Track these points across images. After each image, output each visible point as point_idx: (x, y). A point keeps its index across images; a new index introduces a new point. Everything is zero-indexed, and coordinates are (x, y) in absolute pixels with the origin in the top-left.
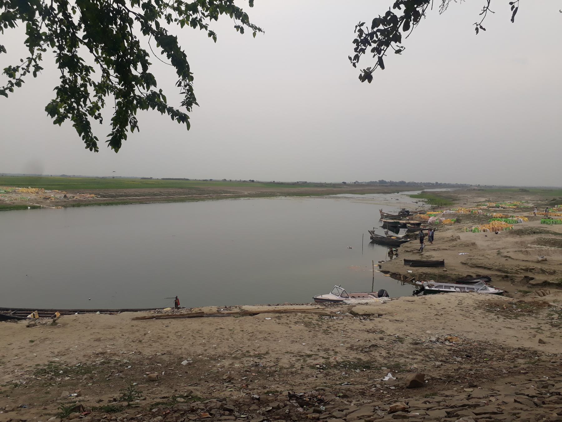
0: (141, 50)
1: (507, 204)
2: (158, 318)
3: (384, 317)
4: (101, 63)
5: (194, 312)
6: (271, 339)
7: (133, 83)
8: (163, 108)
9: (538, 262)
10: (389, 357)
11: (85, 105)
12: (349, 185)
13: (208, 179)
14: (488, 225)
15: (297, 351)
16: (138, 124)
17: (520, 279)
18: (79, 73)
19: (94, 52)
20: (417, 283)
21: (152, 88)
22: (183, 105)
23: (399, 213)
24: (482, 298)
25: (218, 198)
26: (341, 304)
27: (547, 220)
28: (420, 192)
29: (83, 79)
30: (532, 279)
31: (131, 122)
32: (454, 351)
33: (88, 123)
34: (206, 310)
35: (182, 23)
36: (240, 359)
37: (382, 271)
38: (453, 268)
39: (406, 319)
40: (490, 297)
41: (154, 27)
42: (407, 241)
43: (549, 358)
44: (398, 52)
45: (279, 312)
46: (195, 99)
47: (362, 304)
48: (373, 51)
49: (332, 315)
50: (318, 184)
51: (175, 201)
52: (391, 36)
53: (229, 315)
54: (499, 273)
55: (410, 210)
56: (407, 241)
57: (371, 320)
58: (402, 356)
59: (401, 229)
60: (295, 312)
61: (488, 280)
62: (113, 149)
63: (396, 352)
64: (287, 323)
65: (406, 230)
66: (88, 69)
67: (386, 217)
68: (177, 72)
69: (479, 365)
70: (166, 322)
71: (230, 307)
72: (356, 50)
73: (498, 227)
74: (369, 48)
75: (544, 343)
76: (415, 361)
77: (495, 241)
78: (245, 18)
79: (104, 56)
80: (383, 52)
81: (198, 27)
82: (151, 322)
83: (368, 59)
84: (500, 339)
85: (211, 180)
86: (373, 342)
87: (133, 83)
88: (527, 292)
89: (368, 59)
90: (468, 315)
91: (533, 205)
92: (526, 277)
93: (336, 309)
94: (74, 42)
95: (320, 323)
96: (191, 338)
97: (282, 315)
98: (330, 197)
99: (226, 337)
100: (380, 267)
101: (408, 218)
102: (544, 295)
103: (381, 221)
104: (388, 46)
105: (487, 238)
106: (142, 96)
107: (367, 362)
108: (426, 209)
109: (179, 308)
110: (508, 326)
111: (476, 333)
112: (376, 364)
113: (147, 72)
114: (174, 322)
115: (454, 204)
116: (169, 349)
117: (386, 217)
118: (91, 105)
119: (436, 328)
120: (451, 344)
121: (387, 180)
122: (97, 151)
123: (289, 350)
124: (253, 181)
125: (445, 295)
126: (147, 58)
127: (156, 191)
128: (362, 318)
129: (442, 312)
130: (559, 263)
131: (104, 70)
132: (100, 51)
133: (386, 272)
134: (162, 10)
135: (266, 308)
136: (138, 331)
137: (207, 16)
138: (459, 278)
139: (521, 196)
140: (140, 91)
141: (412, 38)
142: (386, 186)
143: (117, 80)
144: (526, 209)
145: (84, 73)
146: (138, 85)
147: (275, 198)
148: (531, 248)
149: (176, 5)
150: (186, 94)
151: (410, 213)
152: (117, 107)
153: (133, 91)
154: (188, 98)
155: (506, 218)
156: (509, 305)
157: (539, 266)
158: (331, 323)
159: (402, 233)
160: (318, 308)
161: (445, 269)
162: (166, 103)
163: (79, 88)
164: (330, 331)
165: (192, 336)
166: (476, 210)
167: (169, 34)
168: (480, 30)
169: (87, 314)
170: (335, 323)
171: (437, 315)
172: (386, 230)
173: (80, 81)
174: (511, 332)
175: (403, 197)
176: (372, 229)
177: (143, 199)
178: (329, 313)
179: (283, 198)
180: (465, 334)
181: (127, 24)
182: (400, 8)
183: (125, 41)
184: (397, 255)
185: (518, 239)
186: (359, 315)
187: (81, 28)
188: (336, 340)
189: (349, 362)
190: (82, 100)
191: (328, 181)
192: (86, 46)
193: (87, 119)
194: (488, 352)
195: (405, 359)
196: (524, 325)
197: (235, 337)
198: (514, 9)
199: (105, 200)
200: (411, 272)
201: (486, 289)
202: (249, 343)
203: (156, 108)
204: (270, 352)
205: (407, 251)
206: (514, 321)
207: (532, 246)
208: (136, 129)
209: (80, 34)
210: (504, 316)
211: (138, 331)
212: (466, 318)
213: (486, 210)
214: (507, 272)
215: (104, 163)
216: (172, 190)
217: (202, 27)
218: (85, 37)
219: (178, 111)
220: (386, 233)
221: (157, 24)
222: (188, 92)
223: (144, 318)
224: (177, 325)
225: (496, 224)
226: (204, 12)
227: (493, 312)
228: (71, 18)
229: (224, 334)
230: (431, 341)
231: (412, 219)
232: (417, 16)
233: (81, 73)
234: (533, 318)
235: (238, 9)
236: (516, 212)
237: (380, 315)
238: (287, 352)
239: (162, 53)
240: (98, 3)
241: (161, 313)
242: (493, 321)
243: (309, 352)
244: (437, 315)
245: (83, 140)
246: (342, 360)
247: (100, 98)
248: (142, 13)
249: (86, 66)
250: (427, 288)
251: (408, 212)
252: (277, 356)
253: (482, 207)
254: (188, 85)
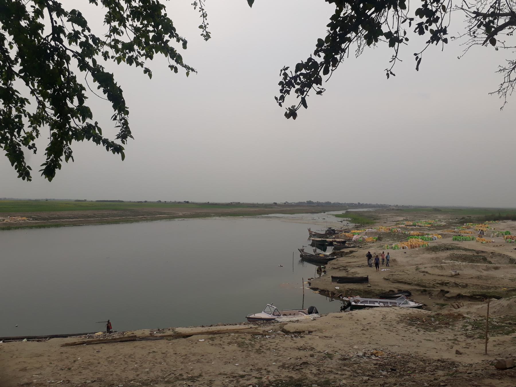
0: (78, 84)
1: (423, 222)
2: (89, 343)
3: (313, 333)
4: (37, 95)
5: (126, 336)
6: (205, 361)
7: (69, 115)
8: (98, 139)
9: (452, 276)
10: (319, 374)
11: (19, 135)
12: (280, 205)
13: (143, 200)
14: (407, 243)
15: (230, 372)
16: (73, 154)
17: (437, 293)
18: (14, 105)
19: (30, 85)
20: (344, 298)
21: (88, 120)
22: (118, 138)
23: (326, 231)
24: (404, 312)
25: (152, 220)
26: (273, 322)
27: (458, 237)
28: (344, 212)
29: (17, 110)
30: (448, 292)
31: (65, 153)
32: (380, 365)
33: (21, 153)
34: (138, 333)
35: (119, 60)
36: (173, 383)
37: (311, 288)
38: (376, 283)
39: (334, 335)
40: (411, 311)
41: (91, 64)
42: (334, 259)
43: (465, 368)
44: (319, 93)
45: (213, 333)
46: (130, 132)
47: (293, 322)
48: (296, 91)
49: (264, 334)
50: (251, 204)
51: (108, 223)
52: (313, 79)
53: (162, 338)
54: (418, 288)
55: (335, 229)
56: (334, 259)
57: (302, 337)
58: (331, 372)
59: (328, 247)
60: (228, 332)
61: (408, 295)
62: (47, 178)
63: (326, 369)
64: (220, 344)
65: (333, 247)
66: (23, 101)
67: (314, 235)
68: (113, 106)
69: (403, 379)
70: (97, 347)
71: (163, 330)
72: (281, 91)
73: (415, 244)
74: (293, 90)
75: (461, 354)
76: (344, 376)
77: (414, 257)
78: (179, 59)
79: (40, 88)
80: (305, 93)
81: (134, 64)
82: (81, 348)
83: (292, 99)
84: (422, 351)
85: (146, 201)
86: (304, 360)
87: (69, 115)
88: (443, 305)
89: (292, 99)
90: (391, 329)
91: (445, 224)
92: (442, 291)
93: (268, 328)
94: (10, 75)
95: (253, 343)
96: (123, 363)
97: (216, 336)
98: (263, 217)
99: (159, 361)
100: (310, 284)
101: (334, 237)
102: (459, 308)
103: (309, 239)
104: (310, 88)
105: (406, 255)
106: (78, 128)
107: (299, 380)
108: (350, 228)
109: (110, 332)
110: (428, 338)
111: (399, 346)
112: (307, 381)
113: (84, 105)
114: (106, 347)
115: (375, 223)
116: (99, 376)
117: (314, 235)
118: (26, 135)
119: (362, 343)
120: (377, 358)
121: (315, 201)
122: (30, 180)
123: (222, 371)
124: (188, 202)
125: (370, 311)
126: (83, 92)
127: (89, 213)
128: (293, 336)
129: (368, 327)
130: (470, 276)
131: (40, 102)
132: (36, 85)
133: (315, 289)
134: (100, 48)
135: (200, 329)
136: (68, 358)
137: (142, 56)
138: (383, 294)
139: (435, 216)
140: (76, 123)
141: (332, 81)
142: (313, 206)
143: (53, 112)
144: (439, 227)
145: (19, 105)
146: (74, 118)
147: (209, 218)
148: (445, 263)
149: (113, 43)
150: (121, 128)
151: (336, 232)
152: (52, 138)
153: (69, 123)
154: (123, 131)
155: (422, 235)
156: (428, 318)
157: (452, 280)
158: (263, 342)
159: (329, 251)
160: (251, 328)
161: (369, 285)
162: (101, 134)
163: (13, 120)
164: (263, 350)
165: (124, 361)
166: (396, 229)
167: (105, 71)
168: (390, 75)
169: (14, 343)
170: (267, 342)
171: (363, 330)
172: (314, 248)
173: (14, 113)
174: (430, 344)
175: (329, 216)
176: (301, 248)
177: (77, 221)
178: (261, 332)
179: (217, 218)
180: (390, 348)
181: (64, 61)
182: (320, 56)
183: (62, 76)
184: (325, 272)
185: (433, 255)
186: (291, 333)
187: (18, 62)
188: (268, 359)
189: (281, 380)
190: (16, 130)
191: (260, 202)
192: (22, 80)
193: (20, 149)
194: (410, 365)
195: (334, 376)
196: (442, 337)
197: (168, 360)
198: (418, 59)
199: (38, 223)
200: (338, 288)
201: (407, 303)
202: (182, 366)
203: (92, 139)
204: (203, 374)
205: (334, 268)
206: (433, 333)
207: (446, 261)
208: (70, 159)
209: (17, 68)
210: (424, 329)
211: (67, 358)
212: (389, 332)
213: (404, 228)
214: (425, 287)
215: (38, 188)
216: (106, 212)
217: (138, 64)
218: (21, 71)
219: (113, 142)
220: (315, 251)
221: (94, 61)
222: (123, 126)
223: (74, 344)
224: (108, 349)
225: (413, 241)
226: (140, 51)
227: (414, 326)
228: (8, 52)
229: (156, 358)
230: (358, 356)
231: (338, 238)
232: (335, 63)
233: (16, 105)
234: (450, 330)
235: (172, 49)
236: (431, 230)
237: (310, 332)
238: (220, 374)
239: (99, 88)
240: (36, 40)
241: (93, 337)
242: (415, 334)
243: (242, 373)
244: (363, 330)
245: (16, 169)
246: (274, 379)
247: (35, 128)
248: (80, 51)
249: (21, 98)
250: (353, 303)
251: (334, 230)
252: (210, 378)
253: (401, 226)
254: (124, 118)
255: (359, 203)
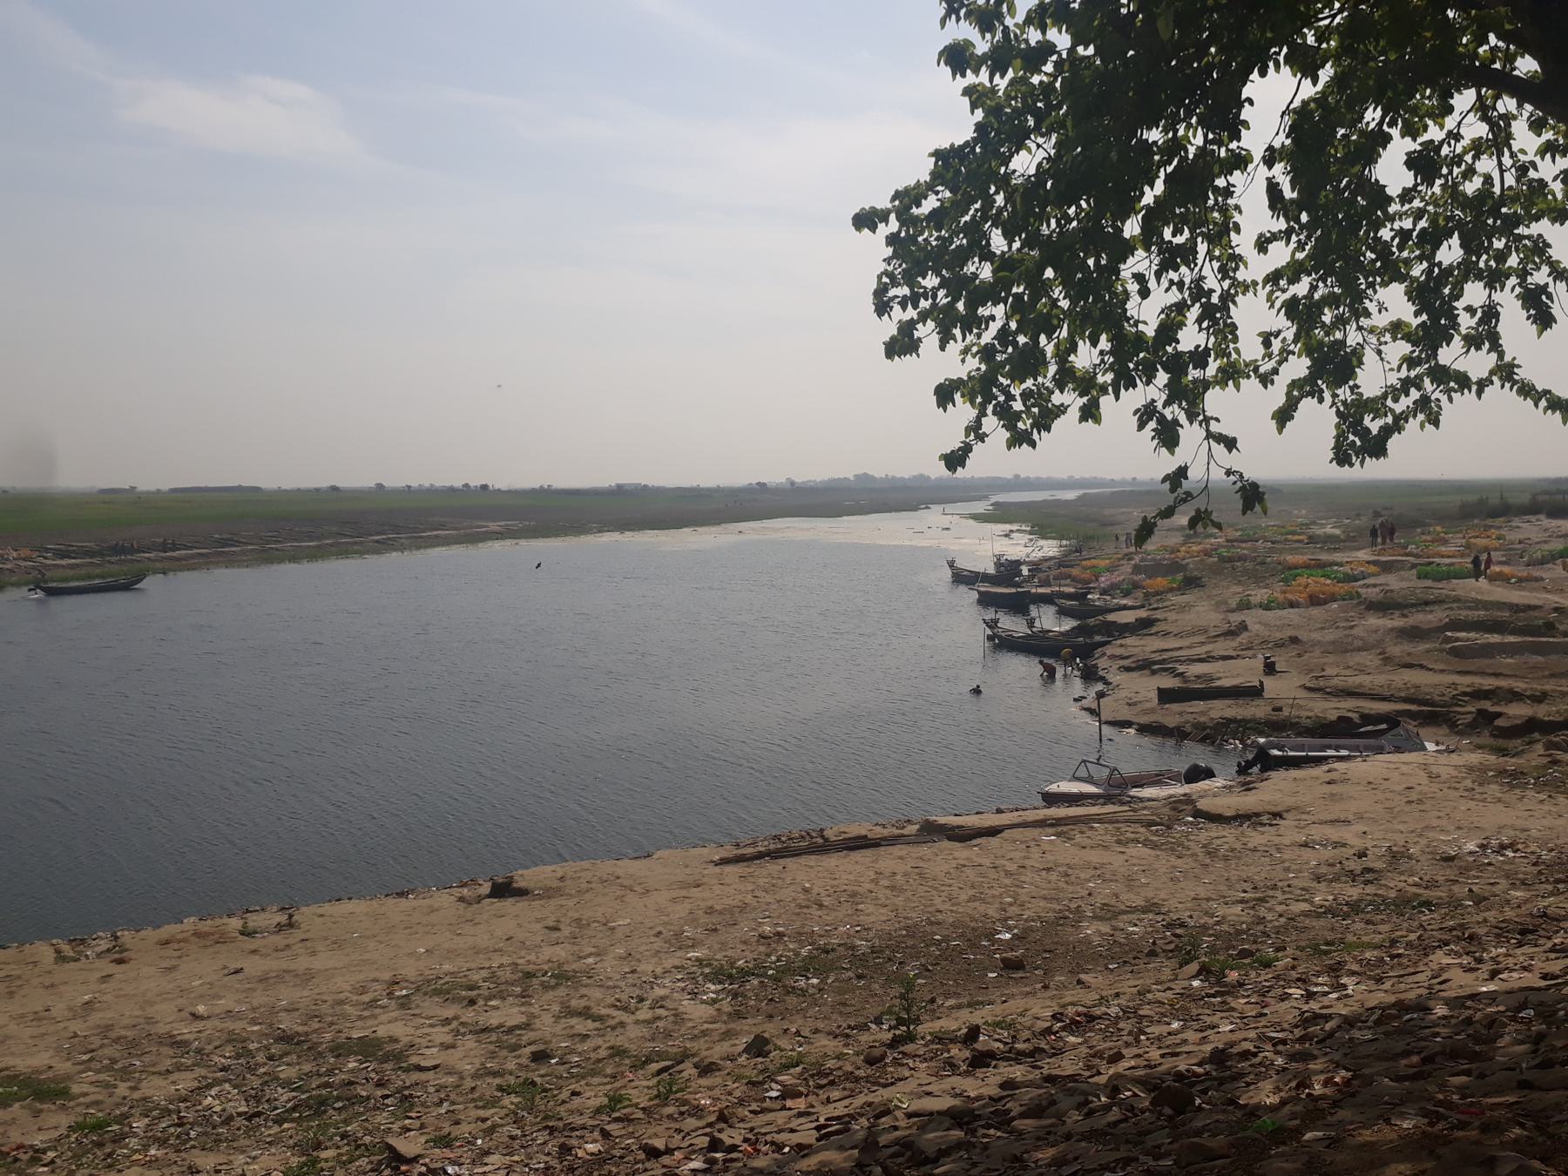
13: (458, 484)
17: (1469, 718)
54: (1413, 708)
85: (484, 487)
92: (1480, 711)
199: (72, 567)
214: (1432, 704)
255: (1017, 476)
